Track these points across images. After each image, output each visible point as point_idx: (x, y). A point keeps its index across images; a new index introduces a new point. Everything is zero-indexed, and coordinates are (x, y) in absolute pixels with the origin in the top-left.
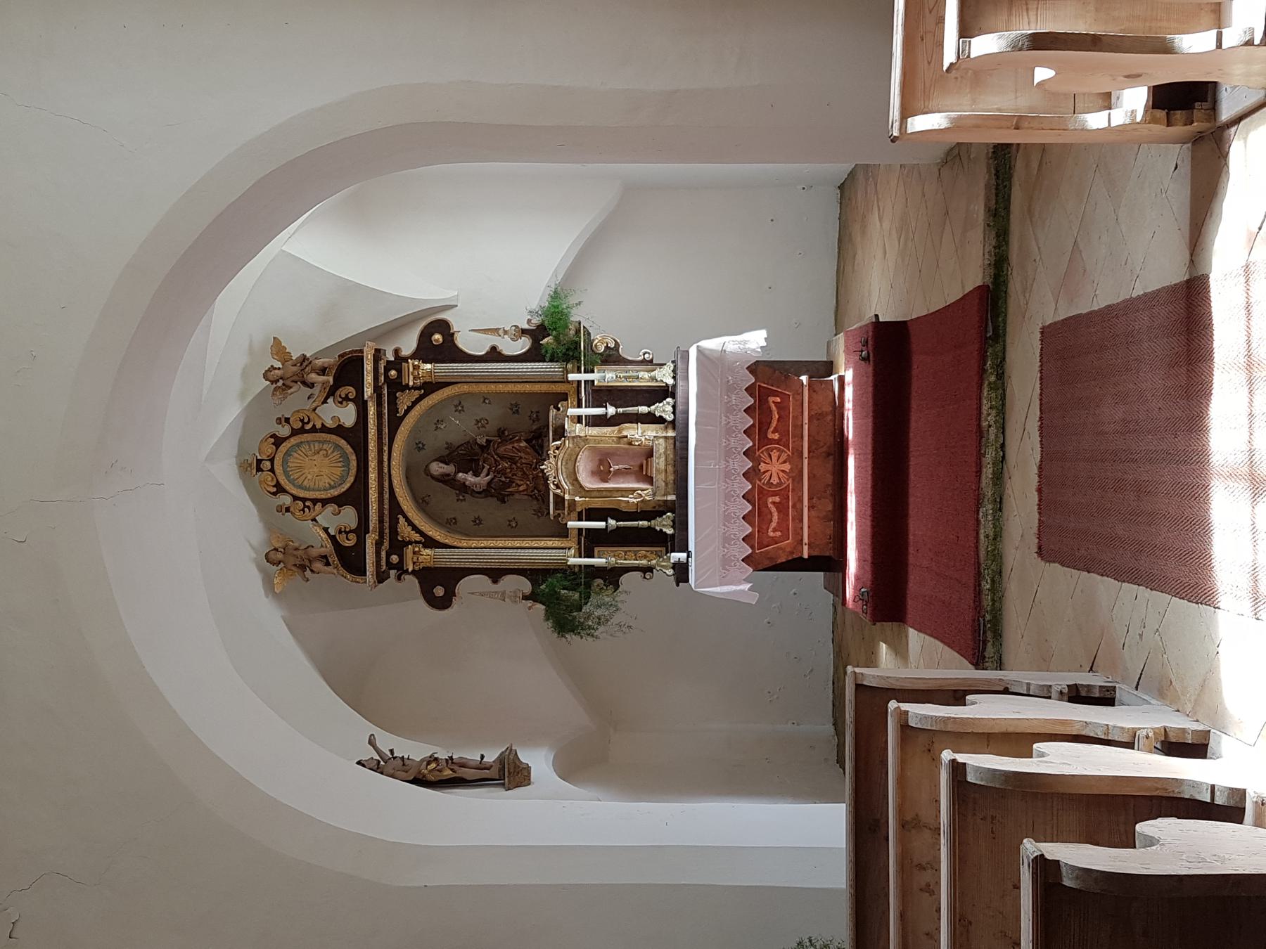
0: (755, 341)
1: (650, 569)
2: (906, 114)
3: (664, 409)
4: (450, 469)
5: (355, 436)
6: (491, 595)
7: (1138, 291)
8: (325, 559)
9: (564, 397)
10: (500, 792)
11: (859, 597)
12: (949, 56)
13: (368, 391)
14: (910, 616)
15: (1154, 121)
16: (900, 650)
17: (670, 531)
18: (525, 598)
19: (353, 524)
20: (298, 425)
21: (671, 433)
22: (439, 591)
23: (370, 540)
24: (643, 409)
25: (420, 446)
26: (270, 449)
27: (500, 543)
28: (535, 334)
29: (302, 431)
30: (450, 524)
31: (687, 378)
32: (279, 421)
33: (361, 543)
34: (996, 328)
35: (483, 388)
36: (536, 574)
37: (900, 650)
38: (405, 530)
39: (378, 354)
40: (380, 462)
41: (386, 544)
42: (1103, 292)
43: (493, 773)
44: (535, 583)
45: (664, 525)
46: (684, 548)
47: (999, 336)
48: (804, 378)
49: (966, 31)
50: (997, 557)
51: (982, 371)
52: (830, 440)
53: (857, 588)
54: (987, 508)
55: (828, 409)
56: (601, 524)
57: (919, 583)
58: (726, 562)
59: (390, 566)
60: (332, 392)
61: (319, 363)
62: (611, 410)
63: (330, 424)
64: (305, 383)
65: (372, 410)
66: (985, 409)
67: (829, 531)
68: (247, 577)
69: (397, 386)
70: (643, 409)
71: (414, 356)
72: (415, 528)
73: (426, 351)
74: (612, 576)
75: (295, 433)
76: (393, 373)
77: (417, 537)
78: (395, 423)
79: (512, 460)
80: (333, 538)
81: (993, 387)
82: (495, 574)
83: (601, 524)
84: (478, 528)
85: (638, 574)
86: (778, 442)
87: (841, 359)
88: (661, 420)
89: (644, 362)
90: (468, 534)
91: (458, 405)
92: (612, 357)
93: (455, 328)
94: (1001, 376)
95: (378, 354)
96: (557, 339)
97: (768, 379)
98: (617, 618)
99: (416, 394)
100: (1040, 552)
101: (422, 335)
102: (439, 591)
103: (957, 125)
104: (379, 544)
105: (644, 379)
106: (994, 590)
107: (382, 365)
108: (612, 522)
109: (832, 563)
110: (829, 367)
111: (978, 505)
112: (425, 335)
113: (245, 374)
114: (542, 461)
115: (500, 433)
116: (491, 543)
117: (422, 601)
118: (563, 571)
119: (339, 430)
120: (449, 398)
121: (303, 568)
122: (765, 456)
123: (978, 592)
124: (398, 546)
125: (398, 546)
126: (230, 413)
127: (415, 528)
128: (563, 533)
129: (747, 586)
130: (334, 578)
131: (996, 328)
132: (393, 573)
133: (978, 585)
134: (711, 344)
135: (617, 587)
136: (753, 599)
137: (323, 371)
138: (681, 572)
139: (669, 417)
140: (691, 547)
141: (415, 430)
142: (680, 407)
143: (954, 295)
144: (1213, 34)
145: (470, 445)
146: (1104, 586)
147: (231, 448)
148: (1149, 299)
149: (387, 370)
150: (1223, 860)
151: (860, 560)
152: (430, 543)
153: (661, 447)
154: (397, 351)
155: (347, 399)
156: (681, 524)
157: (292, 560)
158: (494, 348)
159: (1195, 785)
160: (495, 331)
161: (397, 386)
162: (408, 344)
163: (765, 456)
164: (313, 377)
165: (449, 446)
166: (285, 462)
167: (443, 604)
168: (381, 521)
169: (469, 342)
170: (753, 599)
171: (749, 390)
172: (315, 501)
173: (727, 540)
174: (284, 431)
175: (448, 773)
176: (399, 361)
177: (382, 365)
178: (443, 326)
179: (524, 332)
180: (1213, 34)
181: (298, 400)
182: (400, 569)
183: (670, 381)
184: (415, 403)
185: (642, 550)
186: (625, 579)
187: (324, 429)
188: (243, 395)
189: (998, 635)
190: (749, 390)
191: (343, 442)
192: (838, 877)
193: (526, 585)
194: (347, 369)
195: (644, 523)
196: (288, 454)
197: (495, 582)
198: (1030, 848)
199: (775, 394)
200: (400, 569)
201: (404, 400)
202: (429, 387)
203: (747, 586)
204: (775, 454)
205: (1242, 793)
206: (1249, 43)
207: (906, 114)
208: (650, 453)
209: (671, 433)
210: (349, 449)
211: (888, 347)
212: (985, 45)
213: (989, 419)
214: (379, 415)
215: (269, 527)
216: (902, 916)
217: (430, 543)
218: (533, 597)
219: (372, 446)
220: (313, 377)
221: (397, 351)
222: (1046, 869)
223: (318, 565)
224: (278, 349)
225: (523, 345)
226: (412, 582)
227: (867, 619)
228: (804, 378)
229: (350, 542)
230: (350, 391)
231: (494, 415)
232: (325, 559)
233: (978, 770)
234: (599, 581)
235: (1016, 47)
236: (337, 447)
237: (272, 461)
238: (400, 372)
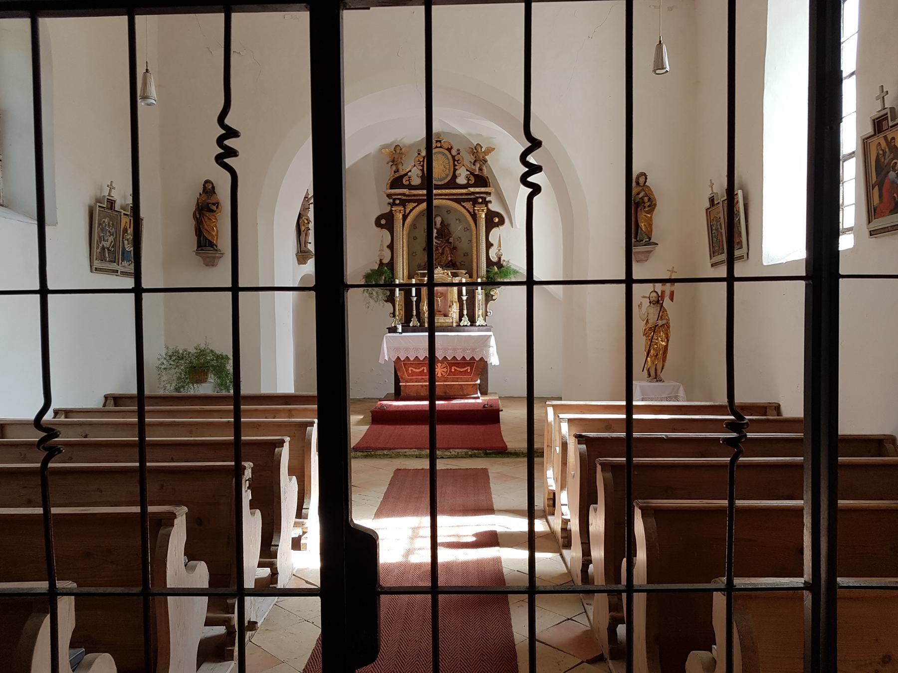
0: (494, 360)
1: (394, 316)
2: (553, 406)
3: (465, 321)
4: (438, 226)
5: (452, 183)
6: (382, 245)
7: (493, 496)
8: (397, 171)
9: (471, 277)
10: (295, 252)
11: (382, 406)
12: (561, 416)
13: (472, 190)
14: (375, 427)
15: (549, 493)
16: (360, 423)
17: (411, 325)
18: (381, 260)
19: (413, 183)
20: (456, 158)
21: (454, 325)
22: (383, 222)
23: (406, 191)
24: (465, 312)
25: (448, 212)
26: (446, 146)
27: (405, 249)
28: (499, 264)
29: (454, 160)
30: (414, 226)
31: (479, 331)
32: (458, 150)
33: (404, 187)
34: (490, 454)
35: (474, 240)
36: (391, 265)
37: (360, 423)
38: (410, 206)
39: (489, 194)
40: (441, 195)
41: (404, 198)
42: (494, 486)
43: (303, 248)
44: (387, 265)
45: (414, 322)
46: (403, 331)
47: (487, 455)
48: (479, 382)
49: (570, 421)
50: (398, 456)
51: (473, 449)
52: (452, 394)
53: (386, 405)
54: (417, 452)
55: (465, 392)
56: (414, 294)
57: (387, 429)
58: (397, 349)
59: (394, 200)
60: (472, 173)
61: (484, 168)
62: (464, 298)
63: (457, 172)
64: (475, 161)
65: (464, 191)
66: (457, 450)
67: (412, 394)
68: (389, 138)
69: (475, 202)
70: (465, 312)
71: (488, 209)
72: (411, 210)
73: (491, 215)
74: (391, 299)
75: (453, 157)
76: (480, 200)
77: (407, 212)
78: (458, 201)
79: (443, 253)
80: (406, 174)
81: (466, 454)
82: (391, 247)
83: (414, 294)
84: (412, 239)
85: (392, 311)
86: (451, 371)
87: (486, 398)
88: (460, 320)
89: (486, 312)
90: (409, 234)
91: (467, 229)
92: (488, 298)
93: (501, 227)
94: (471, 456)
95: (489, 194)
96: (496, 273)
97: (480, 367)
98: (372, 301)
99: (471, 211)
100: (398, 470)
101: (498, 213)
102: (383, 222)
103: (549, 424)
104: (404, 194)
105: (479, 312)
106: (384, 455)
107: (484, 195)
108: (415, 299)
109: (398, 395)
110: (484, 393)
111: (418, 448)
112: (498, 215)
113: (479, 135)
114: (442, 267)
115: (455, 248)
116: (405, 244)
117: (379, 214)
118: (393, 277)
119: (454, 177)
120: (470, 225)
121: (393, 161)
122: (444, 365)
123: (383, 449)
124: (403, 203)
125: (403, 203)
126: (461, 130)
127: (411, 210)
128: (410, 277)
129: (386, 358)
130: (388, 175)
131: (490, 454)
132: (391, 201)
133: (385, 449)
134: (493, 342)
135: (386, 301)
136: (381, 361)
137: (480, 170)
138: (393, 330)
139: (462, 324)
140: (404, 334)
141: (456, 210)
142: (466, 328)
143: (505, 439)
144: (566, 503)
145: (449, 234)
146: (384, 489)
147: (446, 129)
148: (490, 499)
149: (482, 198)
150: (285, 499)
151: (399, 406)
152: (405, 217)
153: (449, 320)
154: (490, 202)
155: (469, 180)
156: (415, 330)
157: (396, 156)
158: (492, 245)
159: (309, 503)
160: (500, 245)
161: (475, 202)
162: (494, 207)
163: (444, 365)
164: (478, 165)
165: (449, 225)
166: (440, 153)
167: (378, 223)
168: (414, 195)
169: (495, 233)
170: (381, 361)
171: (473, 358)
172: (423, 166)
173: (407, 349)
174: (454, 152)
175: (303, 228)
176: (486, 203)
177: (484, 195)
178: (502, 222)
179: (500, 258)
180: (566, 503)
181: (467, 158)
182: (393, 204)
183: (477, 324)
184: (467, 210)
185: (403, 312)
186: (390, 305)
187: (455, 170)
188: (469, 134)
189: (366, 457)
190: (473, 358)
191: (449, 178)
192: (265, 390)
193: (386, 260)
194: (481, 180)
195: (415, 313)
196: (444, 154)
197: (388, 247)
198: (287, 439)
199: (471, 369)
200: (393, 204)
201: (468, 205)
202: (474, 216)
203: (386, 358)
204: (445, 370)
205: (307, 518)
206: (563, 514)
207: (553, 406)
208: (446, 315)
209: (454, 325)
210: (446, 181)
211: (490, 416)
212: (565, 427)
213: (453, 452)
214: (462, 194)
215: (411, 146)
216: (256, 410)
217: (405, 217)
218: (381, 264)
219: (448, 191)
220: (478, 165)
221: (490, 202)
222: (281, 443)
223: (394, 168)
224: (490, 150)
225: (494, 258)
226: (387, 209)
227: (373, 409)
228: (479, 382)
229: (405, 182)
230: (472, 181)
231: (463, 245)
232: (397, 171)
233: (312, 430)
234: (388, 293)
235: (563, 437)
236: (447, 175)
237: (441, 147)
238: (481, 203)
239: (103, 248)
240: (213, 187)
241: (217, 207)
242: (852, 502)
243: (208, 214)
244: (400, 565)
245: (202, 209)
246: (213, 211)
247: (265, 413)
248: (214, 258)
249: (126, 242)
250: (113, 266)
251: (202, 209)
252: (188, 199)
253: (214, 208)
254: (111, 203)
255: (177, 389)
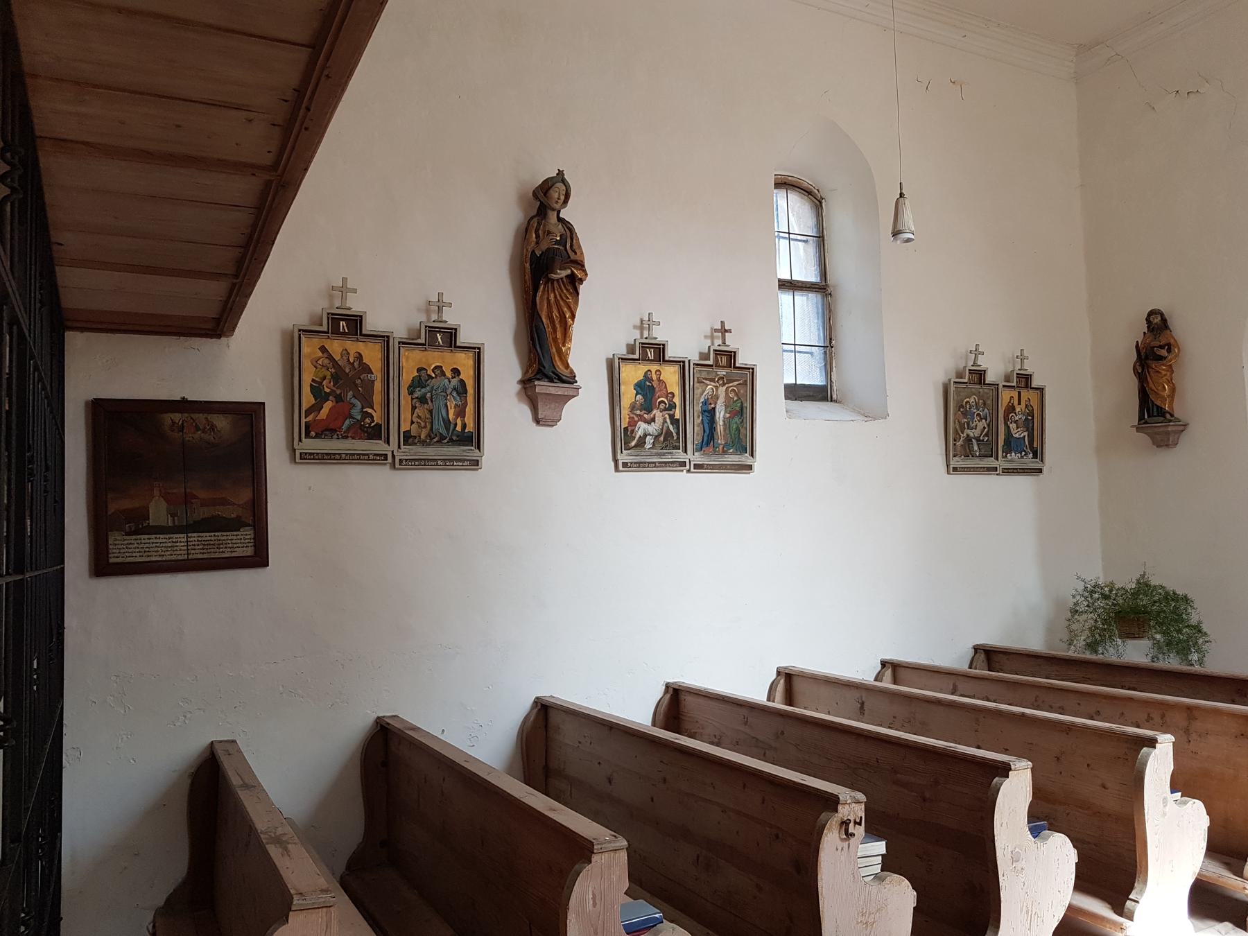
143: (627, 885)
239: (968, 439)
240: (1164, 320)
241: (1169, 351)
242: (1107, 725)
243: (1153, 364)
244: (251, 829)
245: (1147, 358)
246: (1161, 358)
247: (1083, 702)
248: (1168, 433)
249: (1013, 426)
250: (990, 462)
251: (1147, 358)
252: (1126, 335)
253: (1164, 352)
254: (980, 375)
255: (1093, 646)
